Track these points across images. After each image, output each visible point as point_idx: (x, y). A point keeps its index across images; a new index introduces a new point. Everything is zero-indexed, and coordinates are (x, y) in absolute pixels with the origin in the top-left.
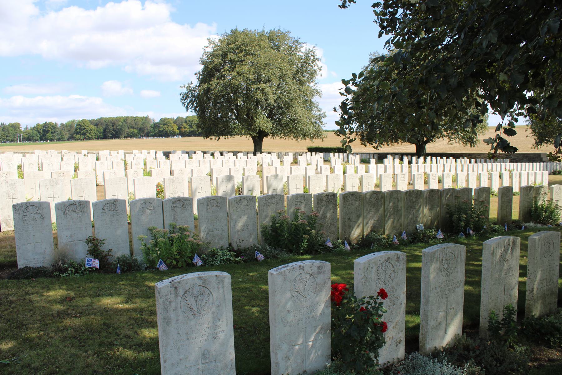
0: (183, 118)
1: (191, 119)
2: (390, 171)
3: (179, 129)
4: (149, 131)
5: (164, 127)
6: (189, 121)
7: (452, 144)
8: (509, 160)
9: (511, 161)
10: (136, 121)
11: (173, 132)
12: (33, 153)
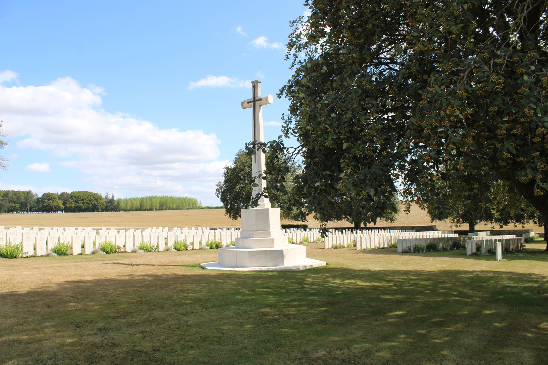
0: (69, 194)
1: (77, 194)
2: (382, 235)
3: (64, 204)
4: (32, 206)
5: (49, 202)
6: (75, 197)
7: (381, 221)
8: (415, 230)
9: (416, 231)
10: (18, 195)
11: (58, 207)
12: (191, 229)
